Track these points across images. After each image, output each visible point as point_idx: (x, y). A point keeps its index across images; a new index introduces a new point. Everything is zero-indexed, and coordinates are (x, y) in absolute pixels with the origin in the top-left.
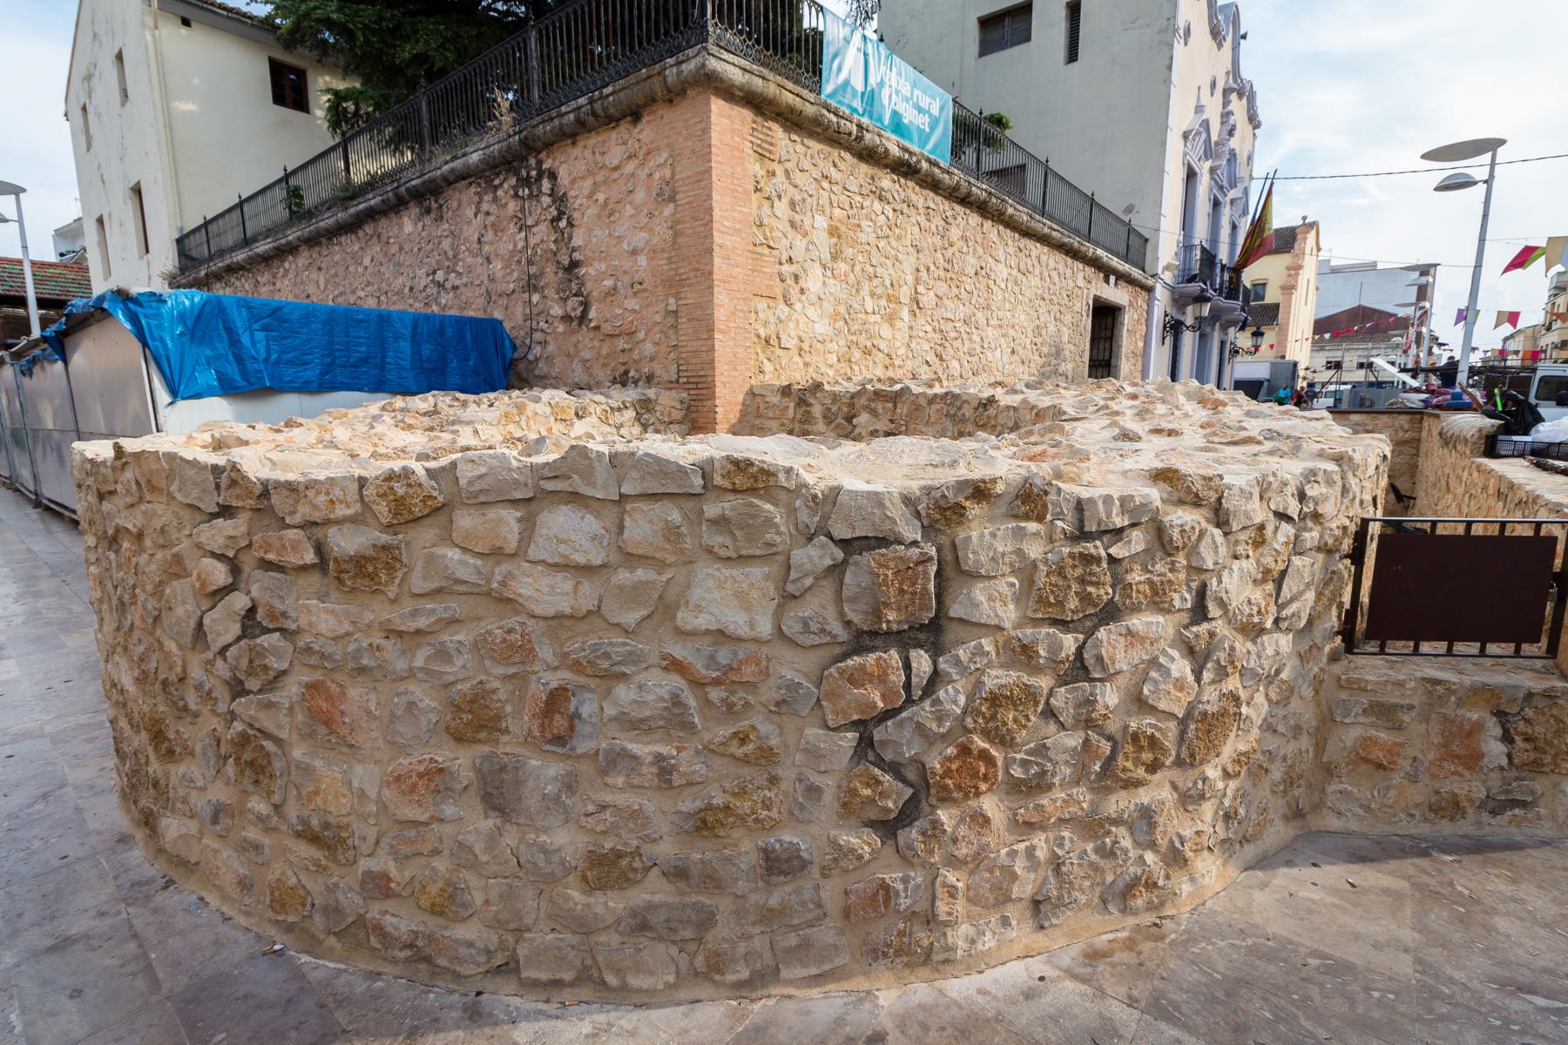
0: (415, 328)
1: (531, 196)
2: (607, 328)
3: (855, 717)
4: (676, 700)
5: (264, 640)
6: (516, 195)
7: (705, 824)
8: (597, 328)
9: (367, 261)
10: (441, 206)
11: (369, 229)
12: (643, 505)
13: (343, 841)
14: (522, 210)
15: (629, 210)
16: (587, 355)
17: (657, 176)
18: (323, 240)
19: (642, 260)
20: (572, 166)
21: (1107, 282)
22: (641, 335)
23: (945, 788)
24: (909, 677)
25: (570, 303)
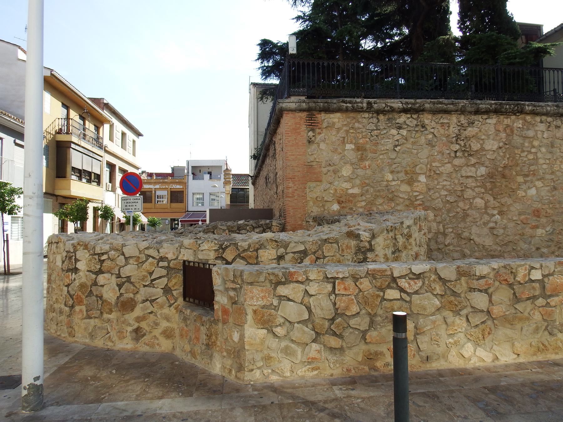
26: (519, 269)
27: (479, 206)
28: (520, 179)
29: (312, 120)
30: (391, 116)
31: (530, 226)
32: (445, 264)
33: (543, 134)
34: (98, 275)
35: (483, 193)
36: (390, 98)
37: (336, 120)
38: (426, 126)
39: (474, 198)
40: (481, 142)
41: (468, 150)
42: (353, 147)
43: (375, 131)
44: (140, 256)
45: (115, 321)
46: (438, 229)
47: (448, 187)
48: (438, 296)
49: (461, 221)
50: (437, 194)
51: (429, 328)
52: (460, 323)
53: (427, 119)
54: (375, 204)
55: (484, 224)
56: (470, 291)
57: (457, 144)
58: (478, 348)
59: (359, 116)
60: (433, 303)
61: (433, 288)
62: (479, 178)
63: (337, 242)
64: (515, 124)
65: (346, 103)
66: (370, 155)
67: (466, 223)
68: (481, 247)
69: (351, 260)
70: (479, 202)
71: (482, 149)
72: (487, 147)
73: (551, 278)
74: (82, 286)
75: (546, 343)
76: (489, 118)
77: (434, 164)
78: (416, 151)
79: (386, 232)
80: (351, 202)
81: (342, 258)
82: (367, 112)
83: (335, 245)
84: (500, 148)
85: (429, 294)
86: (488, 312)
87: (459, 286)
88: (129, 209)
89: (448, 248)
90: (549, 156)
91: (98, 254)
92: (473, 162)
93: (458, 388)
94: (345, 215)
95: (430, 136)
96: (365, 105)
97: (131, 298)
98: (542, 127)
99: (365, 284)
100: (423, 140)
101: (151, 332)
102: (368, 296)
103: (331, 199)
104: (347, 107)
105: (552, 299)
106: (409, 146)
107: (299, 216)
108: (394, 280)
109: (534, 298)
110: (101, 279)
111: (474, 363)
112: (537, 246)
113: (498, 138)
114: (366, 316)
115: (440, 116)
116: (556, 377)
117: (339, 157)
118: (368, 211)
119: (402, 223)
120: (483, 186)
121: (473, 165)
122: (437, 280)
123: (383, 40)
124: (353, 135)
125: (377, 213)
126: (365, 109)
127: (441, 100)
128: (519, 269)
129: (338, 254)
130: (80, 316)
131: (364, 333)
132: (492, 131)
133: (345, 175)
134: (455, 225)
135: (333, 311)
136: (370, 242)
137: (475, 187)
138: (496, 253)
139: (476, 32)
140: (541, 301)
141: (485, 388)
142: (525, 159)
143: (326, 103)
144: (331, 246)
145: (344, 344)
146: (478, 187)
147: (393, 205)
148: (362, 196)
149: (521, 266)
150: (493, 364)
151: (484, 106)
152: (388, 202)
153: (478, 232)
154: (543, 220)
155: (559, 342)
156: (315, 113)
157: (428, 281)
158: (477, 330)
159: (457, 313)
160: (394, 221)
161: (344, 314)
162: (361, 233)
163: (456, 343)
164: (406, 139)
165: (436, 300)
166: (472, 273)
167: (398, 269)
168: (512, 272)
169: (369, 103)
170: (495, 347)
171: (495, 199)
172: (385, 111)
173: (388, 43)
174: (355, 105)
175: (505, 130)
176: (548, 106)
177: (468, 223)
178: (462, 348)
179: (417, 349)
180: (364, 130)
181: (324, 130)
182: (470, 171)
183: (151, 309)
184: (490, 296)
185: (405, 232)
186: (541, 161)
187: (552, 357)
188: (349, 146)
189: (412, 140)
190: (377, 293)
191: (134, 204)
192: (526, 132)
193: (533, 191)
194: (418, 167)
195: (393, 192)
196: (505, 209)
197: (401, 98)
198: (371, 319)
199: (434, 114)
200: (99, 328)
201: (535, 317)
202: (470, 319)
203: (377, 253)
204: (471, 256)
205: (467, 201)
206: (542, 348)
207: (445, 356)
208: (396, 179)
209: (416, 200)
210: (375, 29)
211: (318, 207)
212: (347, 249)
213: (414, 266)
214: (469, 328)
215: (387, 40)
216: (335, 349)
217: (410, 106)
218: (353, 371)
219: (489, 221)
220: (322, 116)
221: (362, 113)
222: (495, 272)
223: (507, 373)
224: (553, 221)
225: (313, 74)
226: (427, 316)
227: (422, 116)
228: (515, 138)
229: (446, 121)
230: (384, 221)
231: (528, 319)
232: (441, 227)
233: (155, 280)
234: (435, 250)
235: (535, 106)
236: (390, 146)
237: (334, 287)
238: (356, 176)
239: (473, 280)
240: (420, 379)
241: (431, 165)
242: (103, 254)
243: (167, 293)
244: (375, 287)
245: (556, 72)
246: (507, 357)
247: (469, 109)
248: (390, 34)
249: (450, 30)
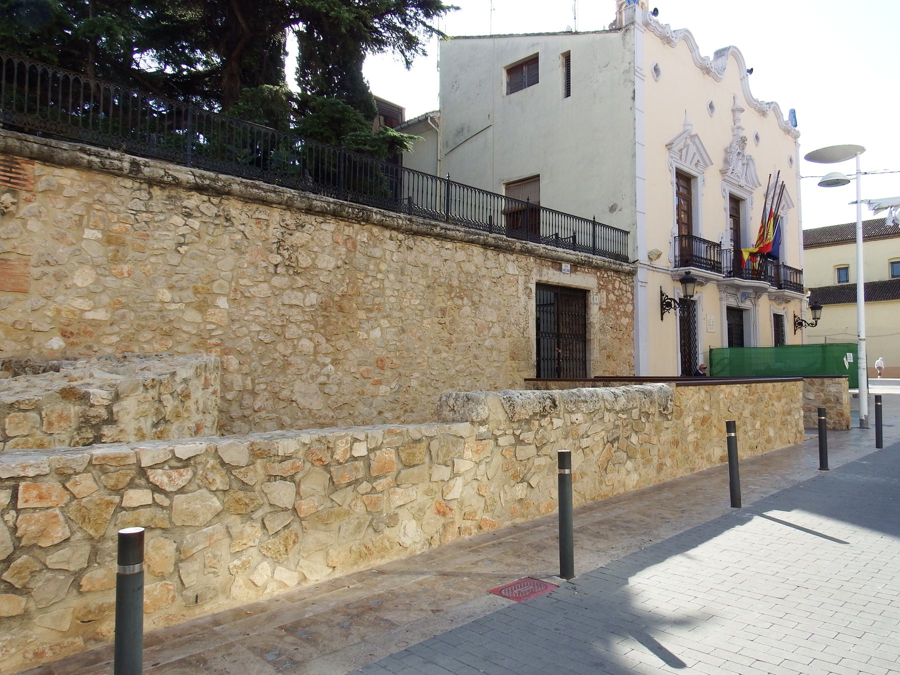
21: (560, 269)
26: (339, 442)
27: (306, 350)
28: (362, 315)
29: (11, 172)
30: (173, 193)
31: (371, 381)
32: (232, 441)
33: (392, 256)
35: (312, 331)
36: (171, 161)
38: (232, 219)
39: (299, 338)
40: (313, 256)
41: (293, 265)
42: (100, 235)
43: (144, 215)
46: (244, 386)
47: (262, 319)
48: (218, 493)
49: (280, 372)
50: (245, 328)
51: (201, 547)
52: (252, 531)
53: (234, 207)
54: (138, 341)
55: (312, 377)
56: (269, 481)
57: (278, 254)
58: (279, 568)
59: (114, 182)
60: (211, 506)
61: (211, 480)
62: (307, 309)
63: (37, 408)
64: (359, 237)
65: (89, 155)
66: (132, 254)
67: (286, 376)
68: (306, 412)
69: (67, 441)
70: (306, 345)
71: (314, 266)
72: (321, 264)
73: (378, 452)
75: (370, 545)
76: (325, 222)
77: (242, 282)
78: (214, 257)
79: (142, 388)
80: (90, 334)
81: (47, 439)
82: (129, 178)
83: (34, 415)
84: (338, 268)
85: (204, 491)
86: (295, 509)
87: (252, 474)
89: (258, 414)
90: (398, 286)
92: (300, 285)
93: (241, 637)
94: (76, 359)
95: (239, 237)
96: (126, 165)
98: (391, 245)
99: (85, 485)
100: (226, 241)
102: (90, 506)
103: (46, 328)
104: (89, 162)
105: (378, 481)
106: (204, 247)
108: (142, 472)
109: (357, 482)
111: (273, 591)
112: (380, 409)
113: (336, 253)
114: (84, 542)
115: (255, 206)
116: (378, 591)
117: (70, 249)
118: (123, 352)
119: (174, 374)
120: (313, 321)
121: (301, 289)
122: (219, 466)
123: (177, 64)
124: (100, 213)
125: (138, 356)
126: (126, 172)
127: (257, 183)
128: (339, 442)
129: (38, 432)
131: (78, 575)
132: (328, 242)
133: (79, 285)
134: (270, 378)
135: (10, 544)
136: (109, 408)
137: (301, 322)
138: (327, 421)
139: (320, 93)
140: (365, 487)
141: (281, 628)
142: (369, 287)
143: (46, 145)
144: (25, 418)
145: (32, 605)
146: (305, 321)
147: (170, 343)
148: (111, 324)
149: (341, 437)
150: (299, 588)
151: (319, 203)
152: (162, 339)
153: (303, 390)
154: (388, 373)
155: (386, 540)
156: (19, 159)
157: (203, 469)
158: (276, 540)
159: (247, 517)
160: (159, 371)
161: (35, 545)
162: (91, 391)
163: (245, 566)
164: (199, 236)
165: (215, 499)
166: (273, 452)
167: (151, 452)
168: (328, 448)
169: (134, 163)
170: (303, 562)
171: (328, 340)
172: (164, 182)
173: (184, 70)
174: (107, 162)
175: (345, 242)
176: (400, 218)
177: (290, 376)
178: (254, 573)
179: (180, 586)
180: (122, 209)
181: (39, 196)
182: (295, 298)
184: (298, 486)
185: (179, 389)
186: (389, 292)
187: (377, 562)
188: (90, 234)
189: (208, 238)
190: (108, 498)
192: (371, 249)
193: (376, 333)
194: (216, 284)
195: (171, 321)
196: (341, 356)
197: (194, 166)
198: (93, 547)
199: (246, 202)
201: (357, 510)
202: (267, 523)
203: (122, 426)
204: (291, 426)
205: (289, 343)
206: (366, 553)
207: (226, 590)
208: (177, 299)
209: (211, 337)
210: (160, 38)
211: (15, 341)
212: (59, 422)
213: (180, 446)
214: (266, 538)
215: (184, 67)
216: (10, 618)
217: (207, 182)
218: (49, 654)
219: (319, 374)
220: (37, 168)
221: (119, 179)
222: (306, 448)
223: (316, 598)
224: (400, 374)
226: (199, 527)
227: (226, 202)
228: (357, 256)
229: (263, 216)
230: (142, 370)
231: (348, 513)
232: (249, 382)
234: (238, 418)
235: (384, 216)
236: (170, 244)
237: (15, 497)
238: (101, 289)
239: (274, 462)
240: (180, 637)
241: (237, 283)
244: (105, 487)
245: (430, 180)
246: (318, 574)
247: (298, 204)
248: (189, 58)
249: (284, 79)
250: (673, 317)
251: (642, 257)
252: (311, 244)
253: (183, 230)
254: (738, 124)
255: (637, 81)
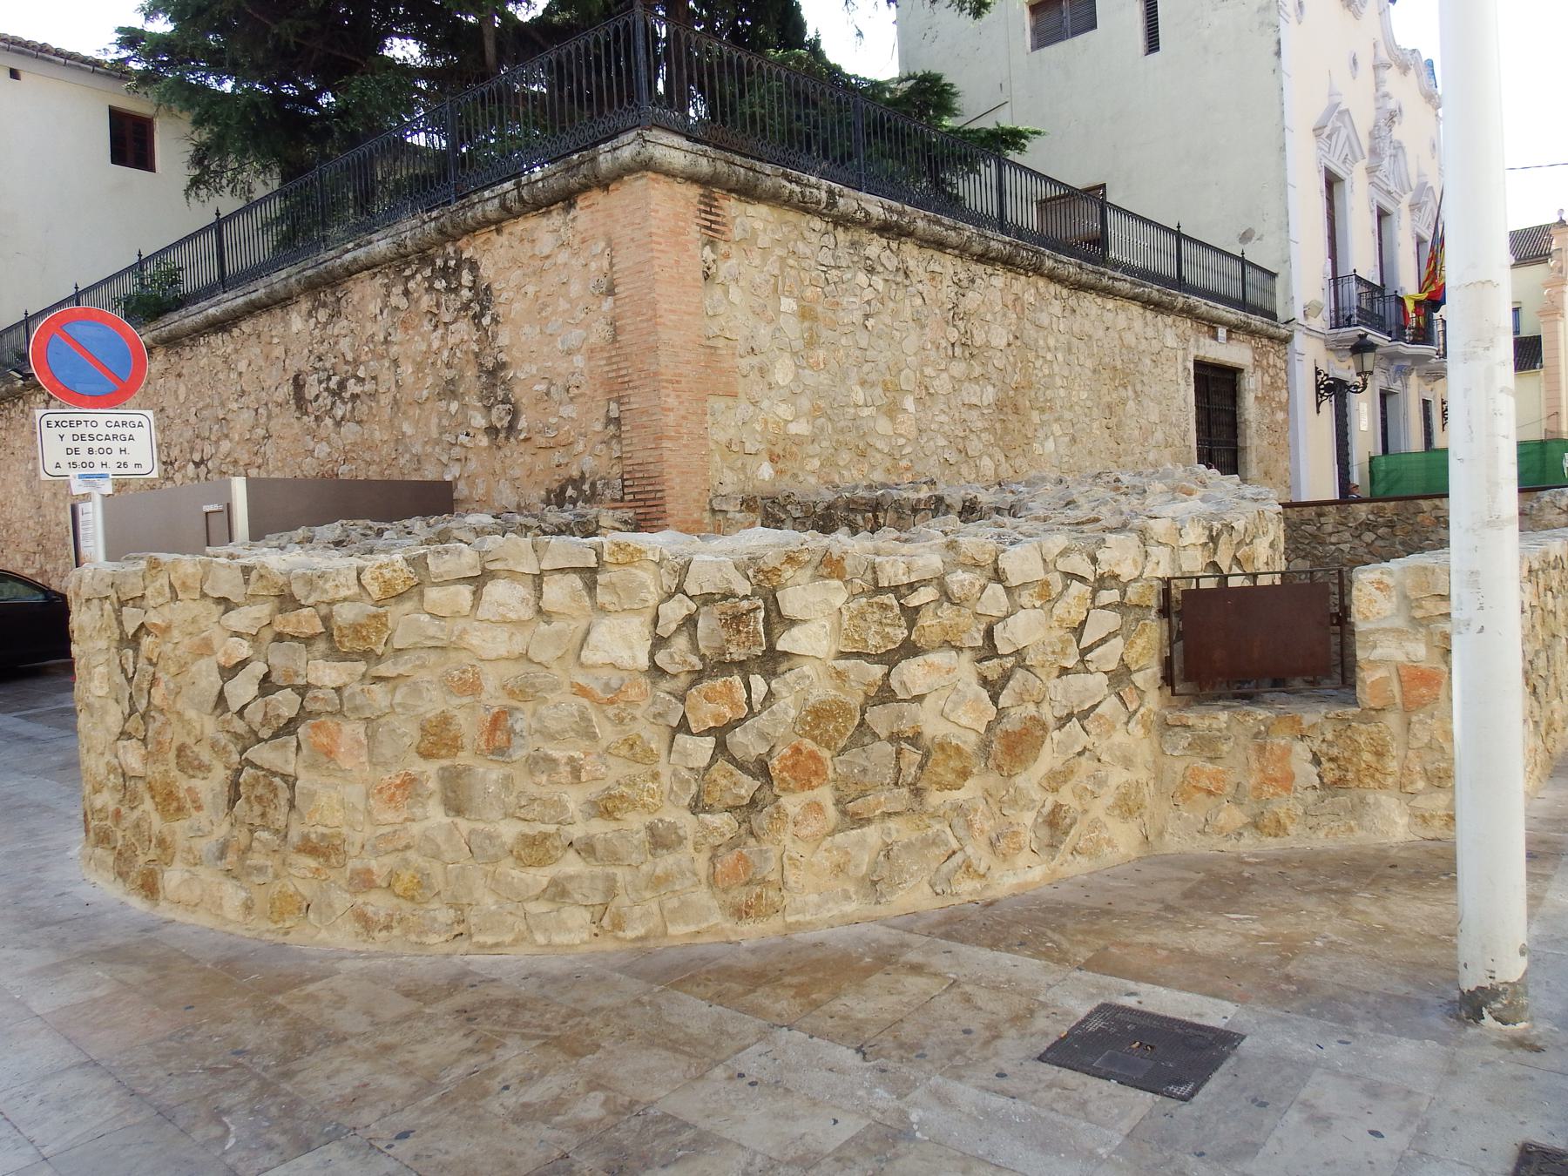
0: (1166, 593)
1: (449, 290)
2: (540, 440)
3: (712, 724)
4: (584, 717)
5: (279, 696)
6: (430, 289)
7: (605, 808)
8: (527, 440)
9: (242, 366)
10: (339, 300)
11: (247, 326)
12: (557, 576)
13: (336, 849)
14: (438, 305)
15: (563, 305)
16: (518, 472)
17: (593, 266)
18: (187, 342)
19: (579, 361)
20: (496, 257)
21: (1215, 338)
22: (580, 447)
23: (783, 780)
24: (749, 697)
25: (494, 411)
29: (710, 213)
34: (892, 665)
37: (759, 225)
44: (1049, 577)
45: (982, 806)
47: (946, 428)
74: (819, 715)
88: (91, 465)
91: (895, 589)
97: (1032, 718)
101: (1085, 811)
107: (695, 494)
110: (912, 674)
115: (930, 252)
130: (813, 827)
174: (808, 191)
183: (1084, 740)
191: (116, 445)
193: (1050, 445)
200: (908, 846)
225: (599, 73)
233: (1090, 649)
236: (857, 317)
242: (912, 587)
243: (1120, 682)
250: (1328, 407)
251: (1298, 314)
252: (982, 310)
253: (868, 294)
254: (1384, 89)
255: (1282, 24)
